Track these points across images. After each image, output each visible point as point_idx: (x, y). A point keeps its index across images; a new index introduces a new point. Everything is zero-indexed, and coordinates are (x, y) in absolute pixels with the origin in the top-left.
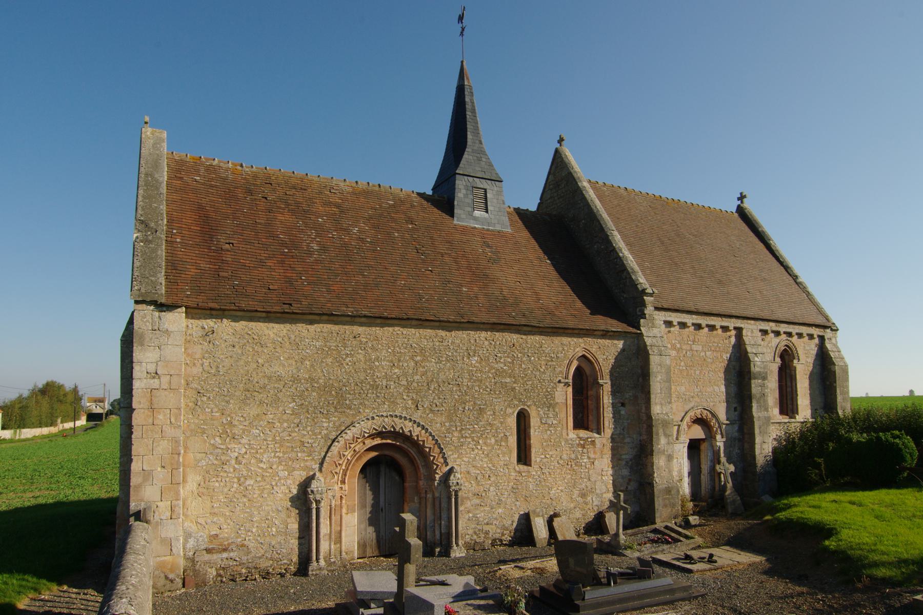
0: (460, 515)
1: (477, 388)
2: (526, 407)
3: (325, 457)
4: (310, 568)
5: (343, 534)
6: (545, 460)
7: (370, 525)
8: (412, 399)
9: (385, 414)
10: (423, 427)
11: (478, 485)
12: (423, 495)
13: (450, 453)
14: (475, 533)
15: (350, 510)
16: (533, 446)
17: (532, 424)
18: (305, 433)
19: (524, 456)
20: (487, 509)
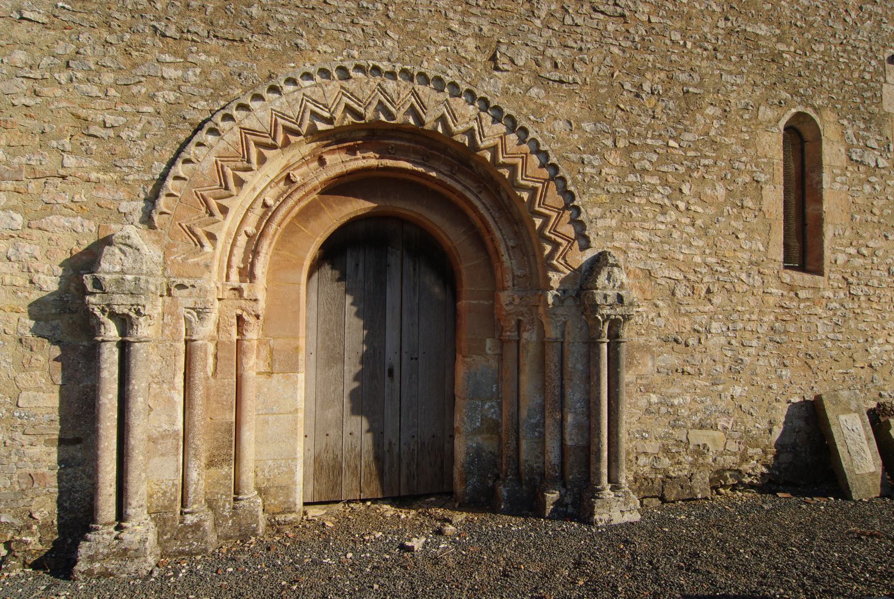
0: (623, 389)
1: (677, 37)
2: (810, 111)
3: (164, 177)
4: (84, 550)
5: (249, 435)
6: (859, 261)
7: (356, 410)
8: (479, 36)
9: (385, 66)
10: (512, 125)
11: (677, 313)
12: (511, 334)
13: (596, 211)
14: (666, 451)
15: (281, 363)
16: (827, 219)
17: (826, 160)
18: (95, 91)
19: (803, 247)
20: (700, 382)
